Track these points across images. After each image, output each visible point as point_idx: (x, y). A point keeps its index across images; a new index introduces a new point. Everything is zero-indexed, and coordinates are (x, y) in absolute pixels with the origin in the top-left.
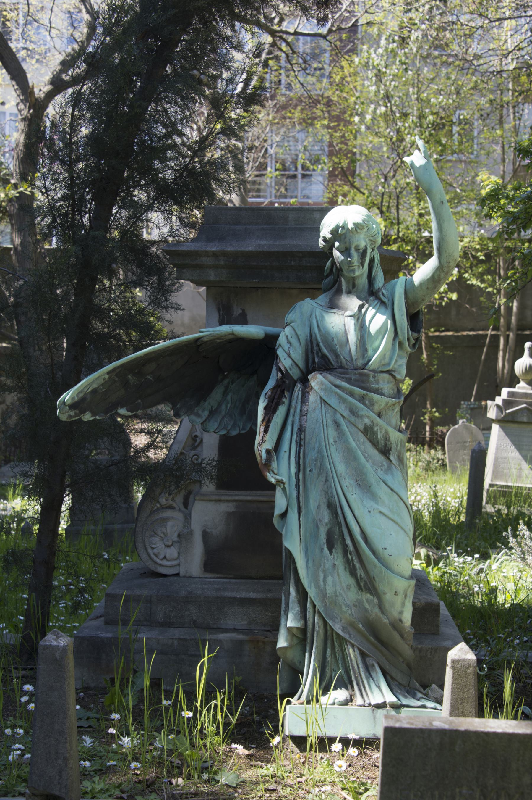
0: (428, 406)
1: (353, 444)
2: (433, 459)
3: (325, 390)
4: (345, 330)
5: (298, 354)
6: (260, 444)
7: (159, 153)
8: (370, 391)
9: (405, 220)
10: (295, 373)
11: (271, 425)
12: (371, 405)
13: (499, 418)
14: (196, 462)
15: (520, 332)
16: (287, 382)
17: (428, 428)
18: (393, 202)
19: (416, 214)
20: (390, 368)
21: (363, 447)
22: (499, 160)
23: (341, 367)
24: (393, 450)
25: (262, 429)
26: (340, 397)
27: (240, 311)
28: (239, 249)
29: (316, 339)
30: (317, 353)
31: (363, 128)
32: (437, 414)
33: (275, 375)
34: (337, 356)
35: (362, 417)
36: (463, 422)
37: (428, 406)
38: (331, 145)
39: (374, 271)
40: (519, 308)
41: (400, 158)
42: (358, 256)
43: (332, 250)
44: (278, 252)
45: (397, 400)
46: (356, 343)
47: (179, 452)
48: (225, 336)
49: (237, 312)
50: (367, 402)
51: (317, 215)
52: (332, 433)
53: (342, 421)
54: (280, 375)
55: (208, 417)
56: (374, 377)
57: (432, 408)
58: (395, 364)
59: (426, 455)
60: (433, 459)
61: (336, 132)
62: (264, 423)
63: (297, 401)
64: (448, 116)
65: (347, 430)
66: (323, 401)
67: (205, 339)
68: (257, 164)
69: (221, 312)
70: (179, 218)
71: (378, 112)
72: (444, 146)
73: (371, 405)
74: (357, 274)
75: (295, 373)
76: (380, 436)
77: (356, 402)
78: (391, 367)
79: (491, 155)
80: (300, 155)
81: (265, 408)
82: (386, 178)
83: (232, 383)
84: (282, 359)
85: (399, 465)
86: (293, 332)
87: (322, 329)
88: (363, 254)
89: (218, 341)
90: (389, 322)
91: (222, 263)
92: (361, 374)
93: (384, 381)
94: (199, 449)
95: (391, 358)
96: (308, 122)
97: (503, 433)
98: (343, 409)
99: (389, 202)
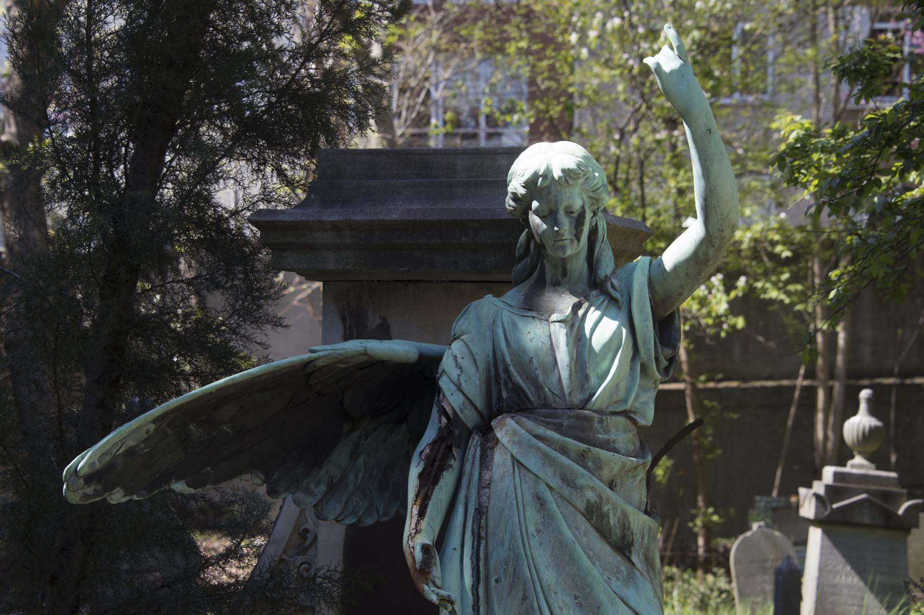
0: (701, 503)
1: (568, 534)
2: (712, 590)
3: (520, 443)
4: (552, 344)
5: (474, 386)
6: (411, 537)
7: (243, 64)
8: (594, 445)
9: (654, 204)
10: (469, 418)
11: (430, 503)
12: (596, 468)
13: (821, 517)
14: (305, 574)
15: (852, 382)
16: (457, 432)
17: (701, 541)
18: (634, 173)
19: (674, 191)
20: (628, 406)
21: (584, 539)
22: (811, 100)
23: (546, 405)
24: (637, 545)
25: (415, 512)
26: (545, 456)
27: (379, 321)
28: (375, 218)
29: (504, 361)
30: (506, 384)
31: (584, 52)
32: (715, 518)
33: (437, 420)
34: (538, 387)
35: (582, 488)
36: (760, 527)
37: (701, 503)
38: (532, 82)
39: (597, 249)
40: (850, 340)
41: (644, 101)
42: (571, 223)
43: (527, 215)
44: (439, 221)
45: (641, 461)
46: (569, 366)
47: (277, 559)
48: (353, 357)
49: (373, 321)
50: (590, 464)
51: (502, 161)
52: (532, 516)
53: (548, 496)
54: (444, 420)
55: (326, 494)
56: (601, 421)
57: (707, 507)
58: (635, 400)
59: (702, 583)
60: (712, 590)
61: (540, 60)
62: (419, 501)
63: (473, 463)
64: (725, 32)
65: (557, 509)
66: (516, 462)
67: (320, 363)
68: (414, 115)
69: (348, 323)
70: (277, 169)
71: (609, 26)
72: (718, 79)
73: (596, 468)
74: (569, 252)
75: (469, 418)
76: (613, 521)
77: (572, 463)
78: (629, 404)
79: (798, 92)
80: (484, 100)
81: (421, 476)
82: (622, 133)
83: (366, 438)
84: (448, 394)
85: (648, 572)
86: (465, 350)
87: (512, 344)
88: (579, 221)
89: (342, 366)
90: (624, 331)
91: (348, 241)
92: (579, 418)
93: (618, 430)
94: (311, 552)
95: (628, 391)
96: (495, 48)
97: (828, 543)
98: (550, 474)
99: (628, 173)
